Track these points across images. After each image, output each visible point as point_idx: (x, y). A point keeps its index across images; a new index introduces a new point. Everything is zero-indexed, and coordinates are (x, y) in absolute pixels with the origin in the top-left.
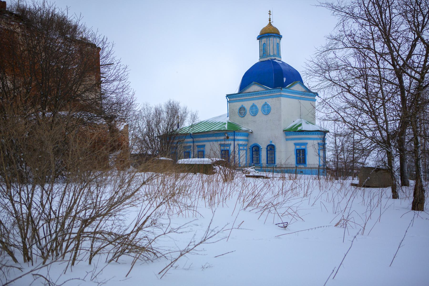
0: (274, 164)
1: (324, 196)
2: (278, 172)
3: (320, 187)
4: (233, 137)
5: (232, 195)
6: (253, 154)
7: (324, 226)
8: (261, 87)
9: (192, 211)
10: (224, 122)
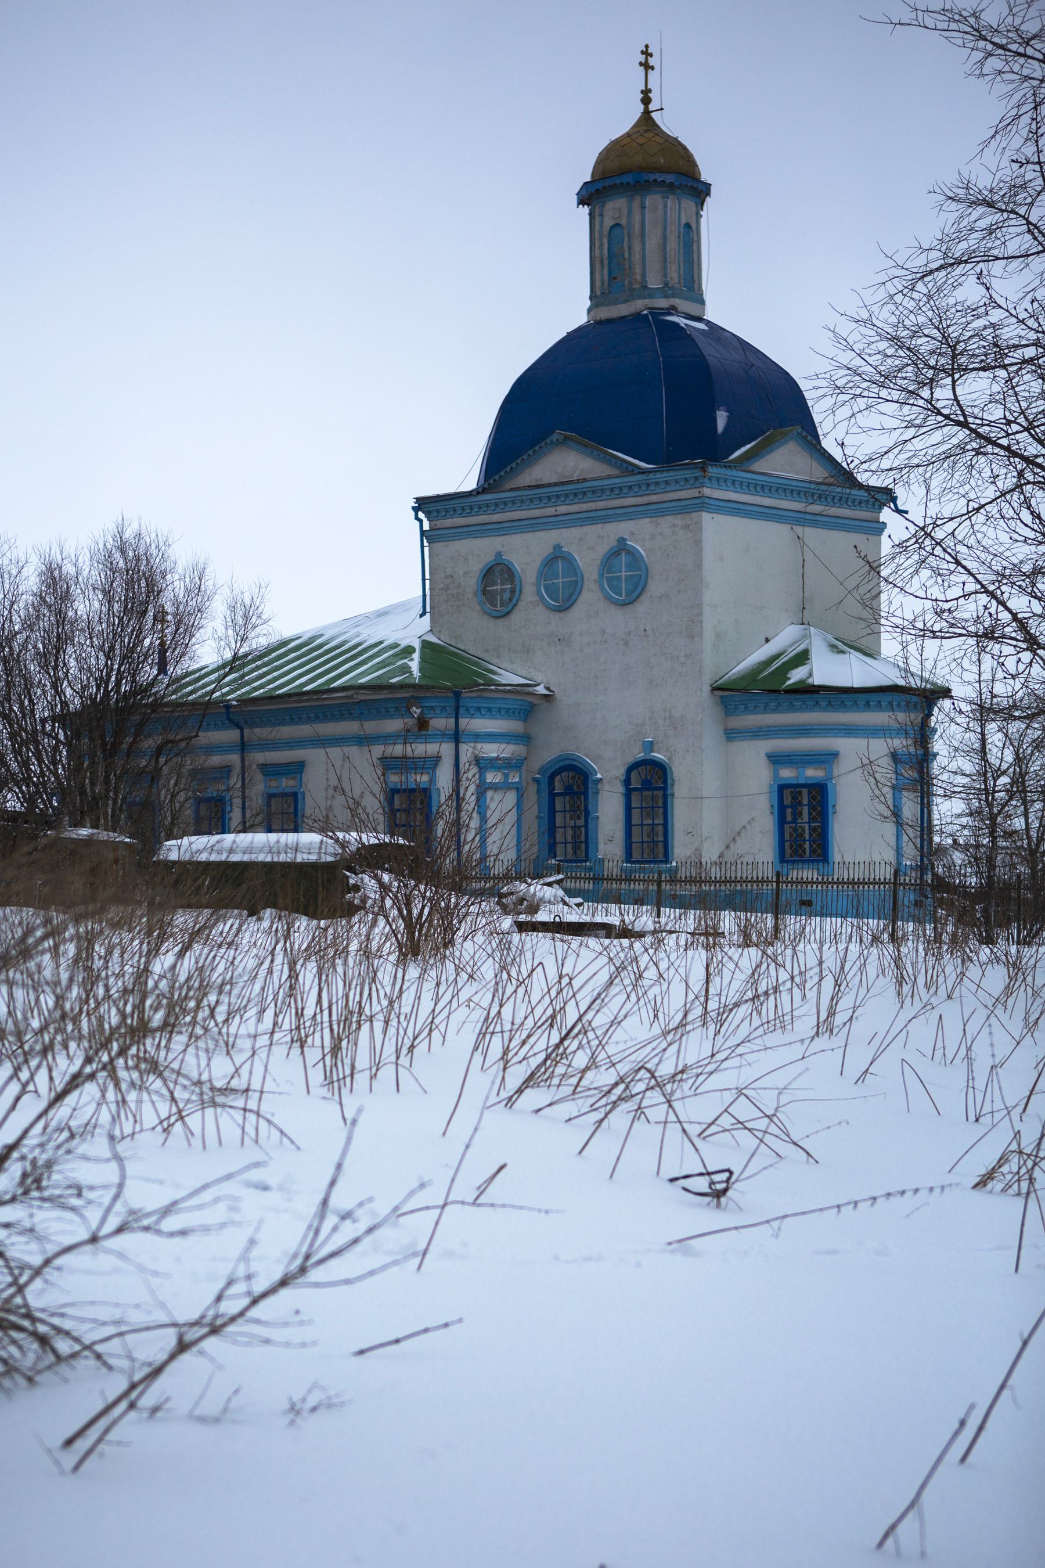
0: (666, 862)
1: (923, 1032)
2: (683, 904)
3: (900, 982)
4: (453, 720)
5: (442, 1027)
6: (552, 812)
7: (916, 1191)
8: (596, 458)
9: (238, 1116)
10: (404, 644)
